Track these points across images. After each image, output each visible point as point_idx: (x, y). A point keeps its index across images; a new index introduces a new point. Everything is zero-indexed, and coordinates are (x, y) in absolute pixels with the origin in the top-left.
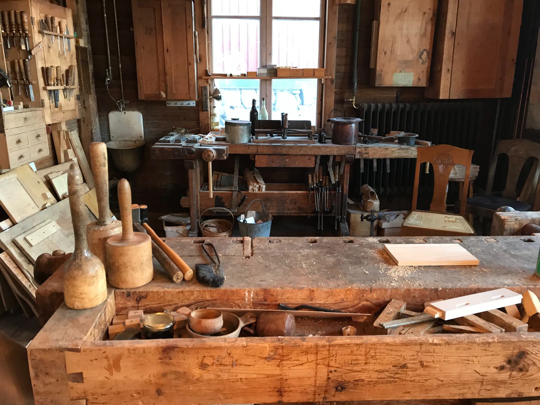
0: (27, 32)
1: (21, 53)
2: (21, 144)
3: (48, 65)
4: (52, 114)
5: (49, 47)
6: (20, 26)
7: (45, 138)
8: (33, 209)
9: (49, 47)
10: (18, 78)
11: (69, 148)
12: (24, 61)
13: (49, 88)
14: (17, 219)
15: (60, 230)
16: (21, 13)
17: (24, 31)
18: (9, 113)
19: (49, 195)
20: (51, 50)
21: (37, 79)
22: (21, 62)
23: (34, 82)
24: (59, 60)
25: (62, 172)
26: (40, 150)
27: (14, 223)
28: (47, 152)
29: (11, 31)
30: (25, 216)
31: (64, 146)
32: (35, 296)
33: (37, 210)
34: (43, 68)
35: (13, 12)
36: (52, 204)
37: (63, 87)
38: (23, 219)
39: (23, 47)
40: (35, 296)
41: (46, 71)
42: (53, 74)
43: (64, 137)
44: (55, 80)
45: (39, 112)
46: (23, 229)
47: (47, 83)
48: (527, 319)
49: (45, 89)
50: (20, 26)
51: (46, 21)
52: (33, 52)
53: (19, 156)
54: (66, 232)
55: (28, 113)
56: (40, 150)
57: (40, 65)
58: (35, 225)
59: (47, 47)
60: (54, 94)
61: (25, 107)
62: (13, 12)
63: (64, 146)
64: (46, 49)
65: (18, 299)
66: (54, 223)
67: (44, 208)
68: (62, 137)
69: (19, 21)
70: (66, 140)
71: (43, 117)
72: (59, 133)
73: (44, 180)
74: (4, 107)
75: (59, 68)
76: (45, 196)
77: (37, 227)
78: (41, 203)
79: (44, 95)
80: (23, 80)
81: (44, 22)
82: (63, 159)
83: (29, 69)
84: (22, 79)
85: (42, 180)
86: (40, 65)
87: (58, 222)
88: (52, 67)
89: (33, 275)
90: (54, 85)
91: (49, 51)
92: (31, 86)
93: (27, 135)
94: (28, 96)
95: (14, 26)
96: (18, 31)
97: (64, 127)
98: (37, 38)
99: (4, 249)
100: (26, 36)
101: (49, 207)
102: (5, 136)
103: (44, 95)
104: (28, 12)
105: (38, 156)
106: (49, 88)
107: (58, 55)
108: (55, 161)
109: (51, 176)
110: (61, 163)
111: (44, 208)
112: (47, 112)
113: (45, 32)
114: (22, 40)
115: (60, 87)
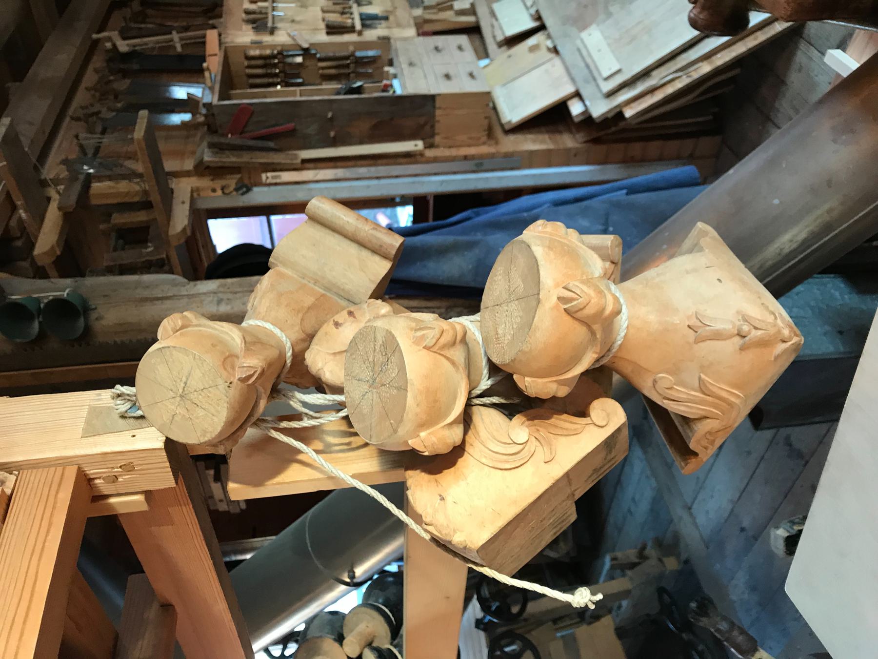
0: (275, 52)
1: (308, 63)
2: (451, 73)
3: (322, 26)
4: (399, 25)
5: (293, 21)
6: (268, 61)
7: (440, 40)
8: (556, 66)
9: (293, 21)
10: (346, 71)
11: (451, 7)
12: (320, 60)
13: (358, 26)
14: (570, 89)
15: (598, 25)
16: (248, 58)
17: (273, 57)
18: (403, 86)
19: (532, 41)
20: (297, 18)
21: (347, 44)
22: (321, 64)
23: (351, 48)
24: (310, 8)
25: (494, 20)
26: (460, 48)
27: (577, 95)
28: (463, 39)
29: (276, 75)
30: (566, 78)
31: (448, 15)
32: (791, 23)
33: (557, 61)
34: (328, 33)
35: (248, 71)
36: (549, 37)
37: (355, 6)
38: (569, 81)
39: (299, 60)
40: (791, 23)
41: (332, 29)
42: (335, 18)
43: (434, 13)
44: (345, 16)
45: (397, 45)
46: (586, 81)
47: (351, 29)
48: (52, 272)
49: (360, 33)
50: (268, 61)
51: (253, 22)
52: (306, 46)
53: (469, 78)
54: (602, 16)
55: (402, 60)
56: (460, 48)
57: (322, 37)
58: (582, 65)
59: (294, 25)
60: (368, 21)
61: (391, 63)
62: (248, 71)
63: (448, 15)
64: (297, 26)
65: (697, 100)
66: (584, 35)
67: (555, 51)
68: (434, 17)
69: (260, 62)
70: (441, 10)
71: (405, 39)
72: (427, 21)
73: (504, 48)
74: (394, 92)
75: (325, 9)
76: (534, 49)
77: (589, 61)
78: (544, 54)
79: (371, 35)
80: (348, 64)
81: (254, 25)
82: (471, 19)
83: (331, 54)
84: (348, 66)
85: (505, 53)
86: (322, 37)
87: (584, 27)
88: (324, 20)
89: (725, 39)
90: (353, 19)
91: (299, 22)
92: (359, 54)
93: (435, 65)
94: (373, 60)
95: (269, 71)
96: (275, 66)
97: (418, 12)
98: (281, 38)
99: (618, 110)
100: (282, 54)
101: (553, 42)
102: (439, 95)
103: (371, 35)
104: (243, 49)
105: (469, 54)
106: (358, 26)
107: (303, 9)
108: (474, 31)
109: (500, 38)
110: (478, 22)
111: (555, 51)
112: (396, 33)
113: (270, 24)
114: (289, 60)
115: (356, 10)
